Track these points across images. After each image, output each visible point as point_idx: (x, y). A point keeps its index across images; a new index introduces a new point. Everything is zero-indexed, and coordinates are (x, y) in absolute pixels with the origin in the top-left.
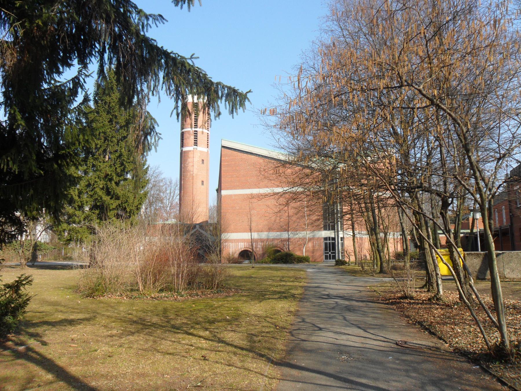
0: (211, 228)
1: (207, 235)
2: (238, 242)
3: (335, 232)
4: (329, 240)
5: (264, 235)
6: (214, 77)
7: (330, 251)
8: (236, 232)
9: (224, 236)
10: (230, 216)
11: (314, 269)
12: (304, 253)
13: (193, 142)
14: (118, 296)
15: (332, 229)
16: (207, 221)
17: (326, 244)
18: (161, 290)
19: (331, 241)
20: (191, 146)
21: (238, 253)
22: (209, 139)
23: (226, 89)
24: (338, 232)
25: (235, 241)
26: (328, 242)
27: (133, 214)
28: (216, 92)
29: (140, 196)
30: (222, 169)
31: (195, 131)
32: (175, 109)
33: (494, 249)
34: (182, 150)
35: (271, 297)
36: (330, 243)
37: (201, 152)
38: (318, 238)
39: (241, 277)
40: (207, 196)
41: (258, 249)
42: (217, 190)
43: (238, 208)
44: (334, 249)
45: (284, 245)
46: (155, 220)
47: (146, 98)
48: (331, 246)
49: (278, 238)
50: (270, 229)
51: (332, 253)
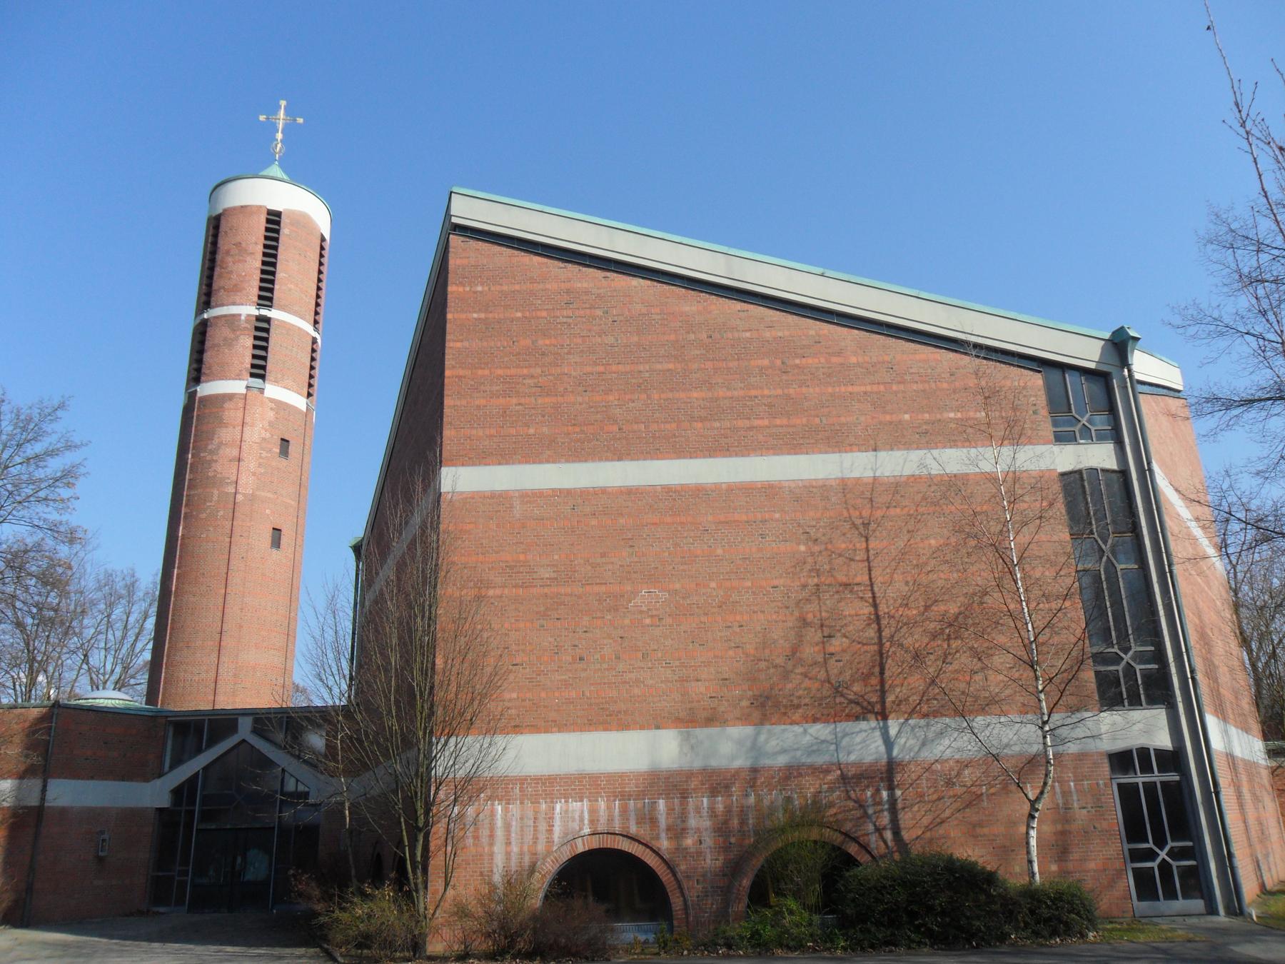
2: (551, 799)
5: (729, 746)
9: (456, 756)
13: (248, 360)
15: (1152, 701)
17: (1128, 794)
19: (1157, 777)
20: (238, 377)
21: (550, 867)
31: (260, 319)
33: (1122, 781)
34: (191, 396)
36: (1150, 788)
37: (280, 406)
38: (1081, 756)
41: (689, 842)
43: (547, 573)
45: (861, 805)
49: (820, 760)
50: (767, 707)
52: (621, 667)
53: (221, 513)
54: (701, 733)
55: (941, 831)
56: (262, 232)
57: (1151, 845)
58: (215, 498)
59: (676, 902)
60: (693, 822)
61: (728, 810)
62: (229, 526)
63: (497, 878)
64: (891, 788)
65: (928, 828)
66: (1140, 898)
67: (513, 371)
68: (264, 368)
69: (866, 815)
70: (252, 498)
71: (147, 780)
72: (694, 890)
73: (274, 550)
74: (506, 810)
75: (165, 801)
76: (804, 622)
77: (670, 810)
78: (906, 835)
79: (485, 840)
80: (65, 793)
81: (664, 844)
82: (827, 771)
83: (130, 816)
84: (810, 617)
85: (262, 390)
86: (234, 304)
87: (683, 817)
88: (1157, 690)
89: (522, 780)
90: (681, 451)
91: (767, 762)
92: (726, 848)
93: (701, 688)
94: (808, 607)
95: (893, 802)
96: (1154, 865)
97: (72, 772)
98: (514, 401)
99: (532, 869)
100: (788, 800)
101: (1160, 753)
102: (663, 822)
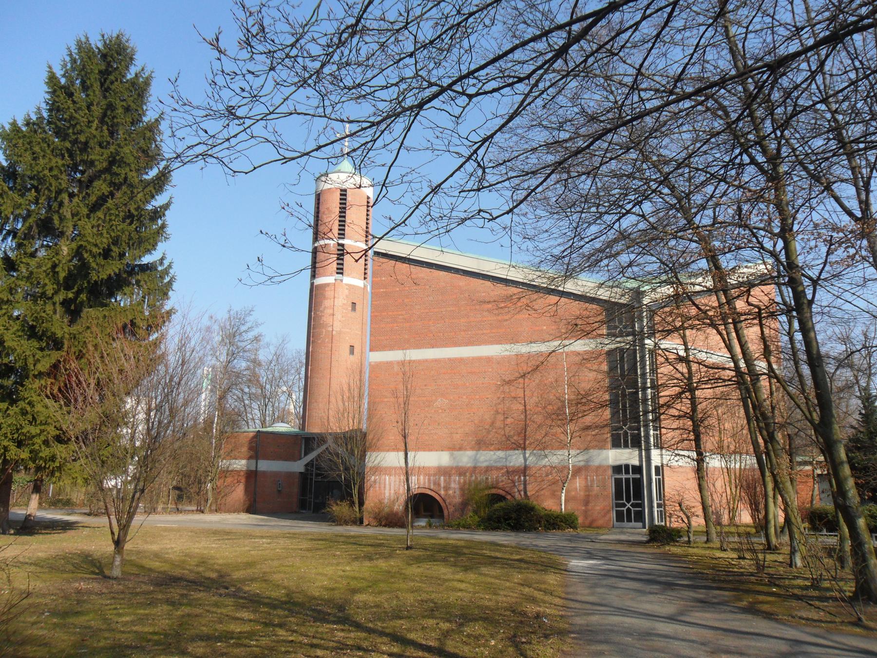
4: (627, 472)
5: (466, 458)
7: (628, 500)
12: (558, 503)
15: (633, 446)
17: (618, 482)
19: (631, 476)
20: (331, 275)
24: (648, 450)
26: (624, 476)
34: (312, 284)
36: (627, 480)
37: (351, 287)
38: (599, 467)
41: (451, 492)
44: (639, 494)
45: (513, 482)
48: (631, 488)
49: (499, 465)
50: (481, 444)
52: (430, 428)
54: (457, 453)
55: (542, 492)
56: (338, 201)
57: (624, 501)
59: (446, 512)
60: (453, 485)
61: (465, 482)
65: (537, 492)
66: (617, 521)
68: (342, 269)
69: (515, 486)
70: (340, 333)
71: (295, 461)
72: (451, 509)
75: (302, 470)
76: (497, 412)
77: (445, 481)
78: (529, 494)
80: (264, 465)
81: (442, 492)
82: (502, 469)
83: (290, 475)
84: (500, 410)
85: (342, 281)
87: (449, 483)
88: (636, 443)
90: (456, 344)
91: (479, 465)
92: (463, 495)
93: (458, 436)
94: (500, 406)
95: (525, 481)
96: (625, 509)
97: (266, 457)
100: (487, 479)
101: (633, 466)
102: (442, 485)
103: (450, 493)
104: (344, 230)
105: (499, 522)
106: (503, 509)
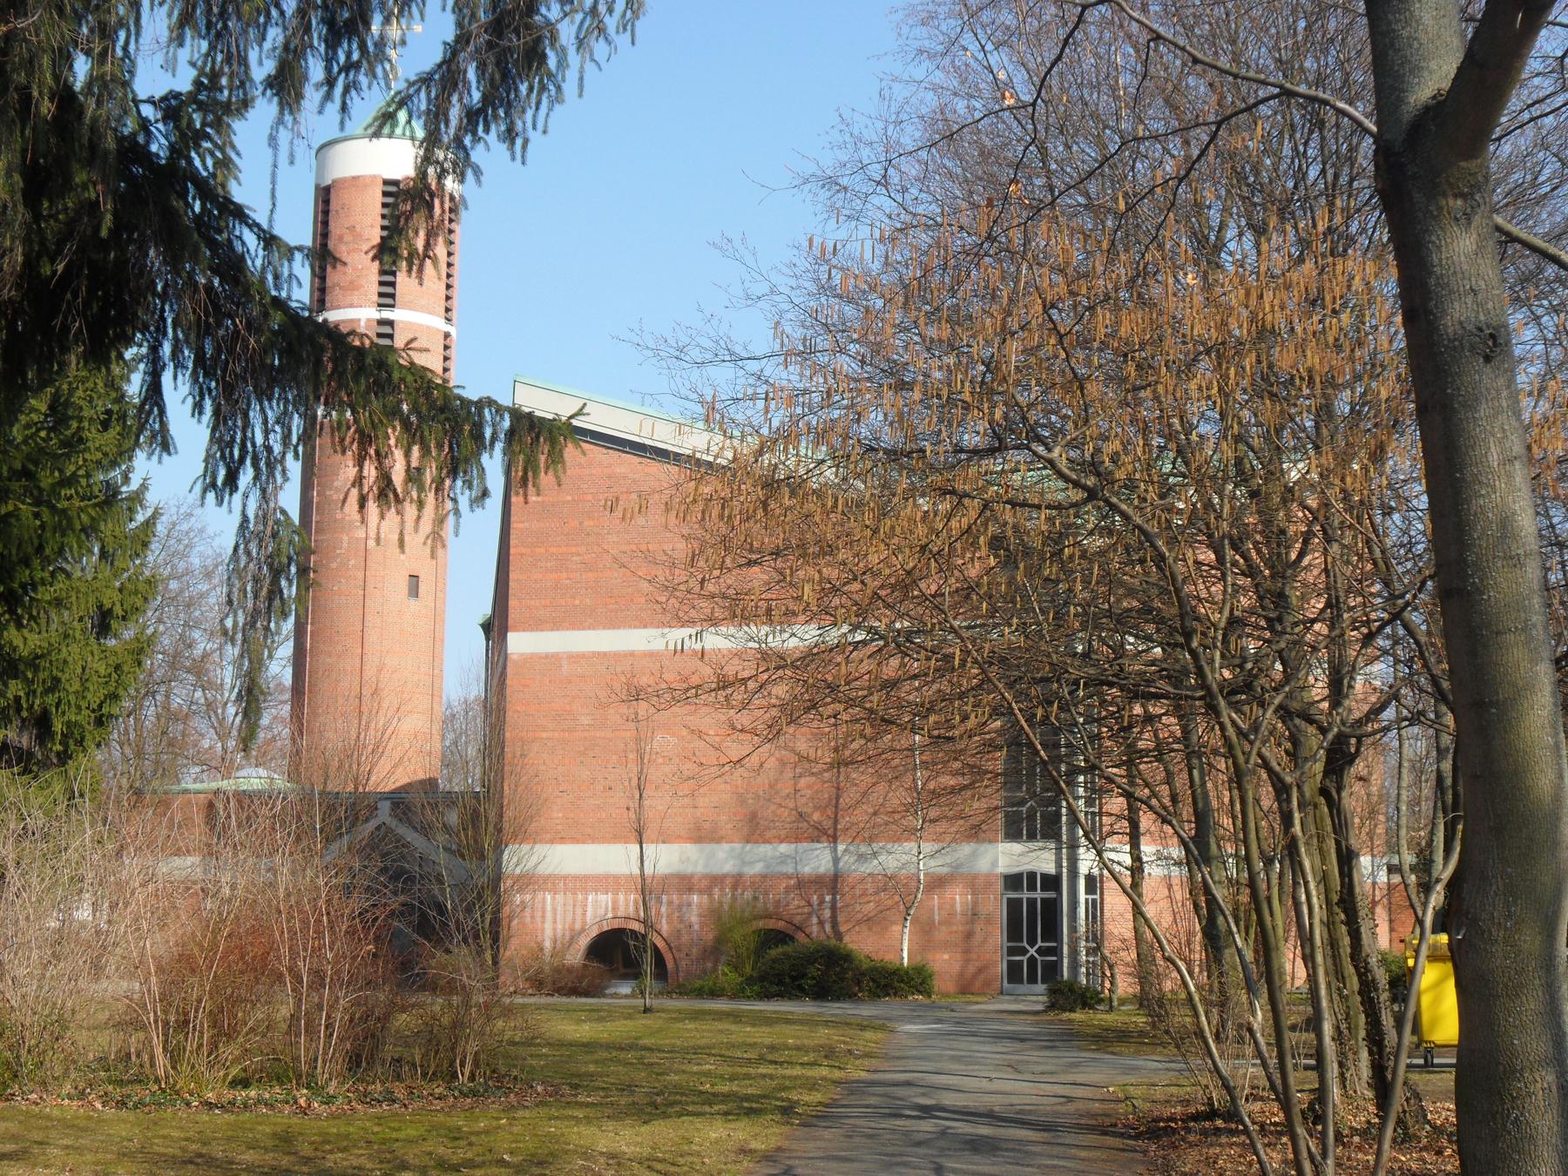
0: (453, 818)
1: (435, 851)
2: (585, 891)
3: (1059, 849)
4: (1032, 887)
5: (723, 858)
6: (469, 382)
7: (1032, 942)
8: (575, 840)
9: (518, 859)
10: (545, 762)
11: (939, 1021)
12: (902, 947)
14: (70, 1098)
15: (1045, 837)
16: (431, 784)
17: (1014, 906)
18: (244, 1083)
19: (1039, 895)
21: (584, 942)
22: (455, 293)
23: (507, 416)
24: (1073, 847)
25: (572, 879)
26: (1025, 895)
27: (80, 742)
28: (478, 428)
29: (112, 660)
30: (516, 525)
31: (381, 322)
32: (353, 485)
35: (698, 1108)
36: (1032, 902)
39: (589, 1046)
40: (435, 657)
42: (487, 627)
43: (585, 720)
44: (1052, 931)
46: (168, 772)
47: (279, 468)
48: (1036, 914)
50: (754, 830)
51: (1040, 951)
53: (352, 562)
58: (345, 545)
62: (361, 576)
63: (548, 944)
64: (834, 895)
67: (564, 549)
73: (412, 601)
74: (553, 899)
79: (539, 919)
86: (351, 306)
88: (1049, 830)
89: (565, 878)
95: (834, 902)
96: (1025, 959)
98: (564, 575)
99: (573, 939)
101: (1045, 877)
103: (681, 923)
104: (393, 284)
105: (781, 983)
106: (787, 956)
